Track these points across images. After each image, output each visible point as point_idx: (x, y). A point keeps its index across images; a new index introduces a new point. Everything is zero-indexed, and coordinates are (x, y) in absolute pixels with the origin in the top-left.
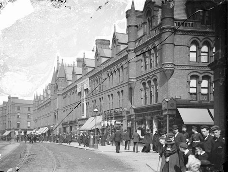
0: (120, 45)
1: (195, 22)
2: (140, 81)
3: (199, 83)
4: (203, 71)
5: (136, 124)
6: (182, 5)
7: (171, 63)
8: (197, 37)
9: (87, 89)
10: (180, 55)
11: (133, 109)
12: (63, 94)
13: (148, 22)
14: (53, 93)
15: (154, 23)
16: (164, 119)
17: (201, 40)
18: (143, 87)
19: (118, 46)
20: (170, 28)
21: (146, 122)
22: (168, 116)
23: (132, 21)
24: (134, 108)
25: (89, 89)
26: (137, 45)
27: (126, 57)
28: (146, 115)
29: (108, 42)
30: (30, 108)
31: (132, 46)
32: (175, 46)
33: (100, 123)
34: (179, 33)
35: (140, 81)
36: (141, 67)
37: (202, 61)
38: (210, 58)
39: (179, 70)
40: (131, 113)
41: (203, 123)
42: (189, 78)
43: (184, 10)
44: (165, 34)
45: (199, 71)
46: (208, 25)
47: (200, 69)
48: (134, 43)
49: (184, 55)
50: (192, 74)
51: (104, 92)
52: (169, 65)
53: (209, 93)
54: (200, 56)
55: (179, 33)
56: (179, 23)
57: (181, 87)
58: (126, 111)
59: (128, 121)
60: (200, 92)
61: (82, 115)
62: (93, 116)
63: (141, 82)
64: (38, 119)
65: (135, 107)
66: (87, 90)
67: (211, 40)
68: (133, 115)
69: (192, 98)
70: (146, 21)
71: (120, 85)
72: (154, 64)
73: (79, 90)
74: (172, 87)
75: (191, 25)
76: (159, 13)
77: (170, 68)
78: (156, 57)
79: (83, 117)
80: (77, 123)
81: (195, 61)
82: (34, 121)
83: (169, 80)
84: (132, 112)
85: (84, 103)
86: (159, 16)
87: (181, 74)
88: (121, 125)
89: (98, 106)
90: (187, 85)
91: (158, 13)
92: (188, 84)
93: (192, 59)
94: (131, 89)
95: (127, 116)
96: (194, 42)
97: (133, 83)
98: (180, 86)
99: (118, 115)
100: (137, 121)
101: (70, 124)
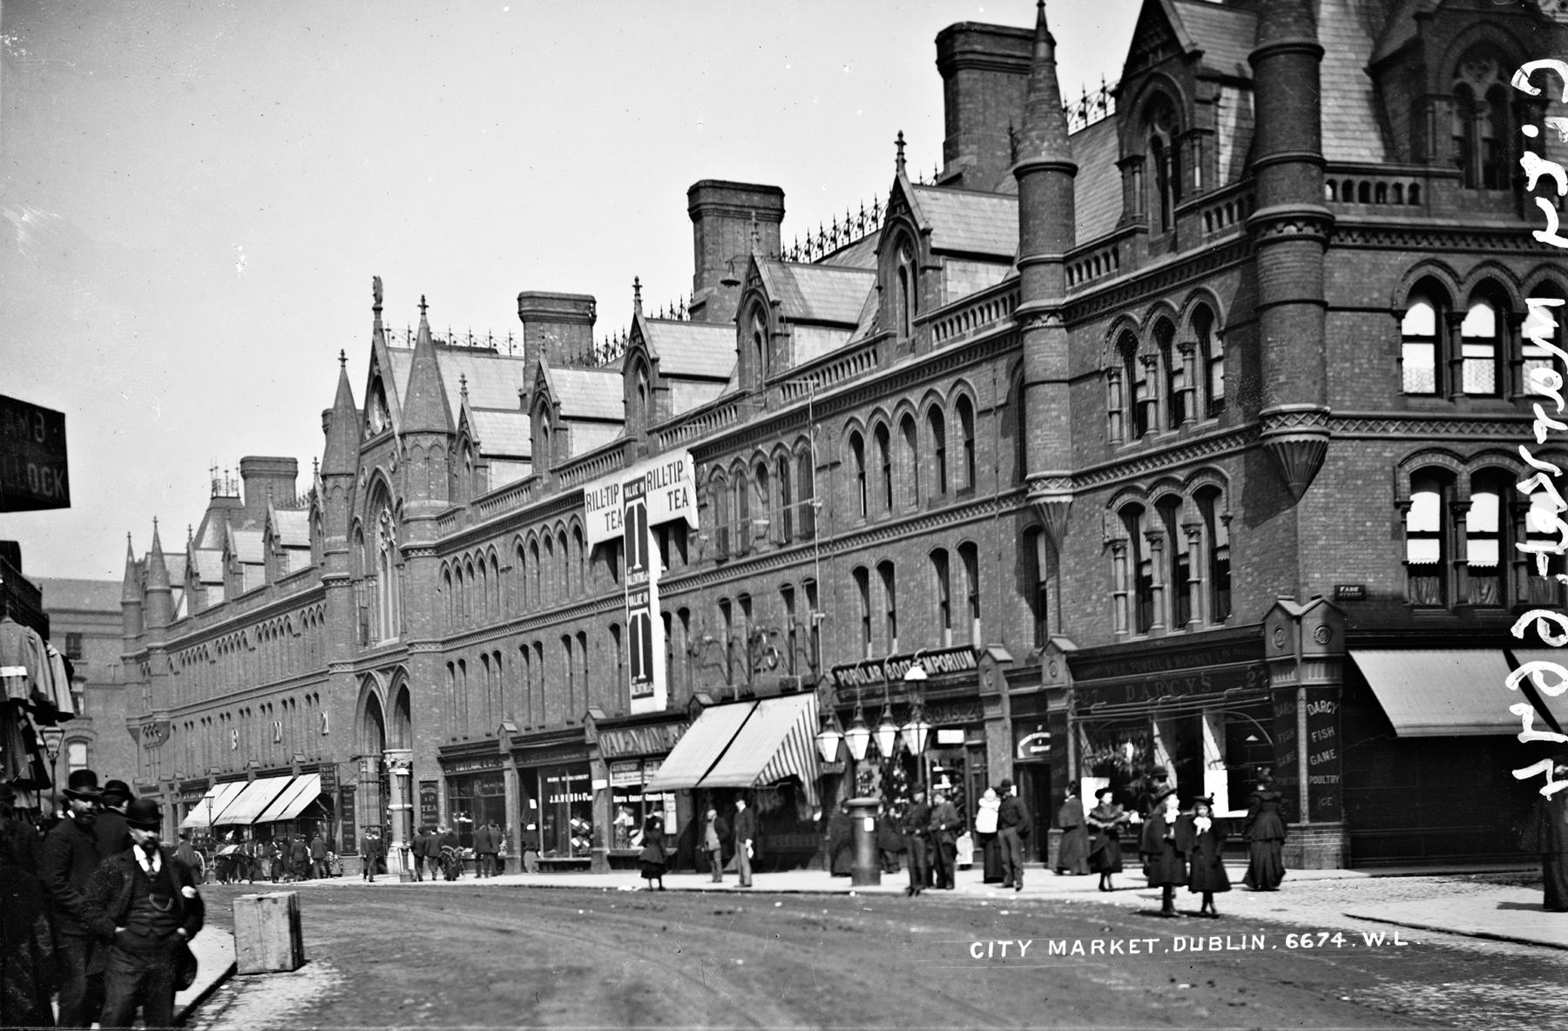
0: (940, 261)
1: (1427, 176)
2: (1106, 495)
3: (1454, 511)
4: (1477, 447)
5: (1084, 742)
6: (1351, 72)
7: (1313, 406)
8: (1442, 257)
9: (680, 525)
10: (1352, 361)
11: (1064, 657)
12: (440, 549)
13: (1150, 161)
14: (344, 538)
15: (1197, 170)
16: (1280, 712)
17: (1461, 272)
18: (1121, 531)
19: (930, 272)
20: (1310, 219)
21: (1156, 731)
22: (1302, 693)
23: (1042, 139)
24: (1065, 652)
25: (694, 522)
26: (1077, 283)
27: (1008, 345)
28: (1153, 689)
29: (773, 199)
30: (79, 636)
31: (1047, 291)
32: (1330, 314)
33: (814, 739)
34: (1349, 242)
35: (1106, 495)
36: (1111, 414)
37: (1467, 389)
38: (1507, 372)
39: (1348, 443)
40: (1047, 677)
41: (1492, 725)
42: (1405, 482)
43: (1365, 104)
44: (1279, 249)
45: (1454, 446)
46: (1494, 188)
47: (1461, 436)
48: (1060, 268)
49: (1375, 362)
50: (1417, 463)
51: (821, 545)
52: (1301, 417)
53: (1509, 563)
54: (1457, 363)
55: (1349, 242)
56: (1348, 186)
57: (1363, 533)
58: (1010, 667)
59: (1020, 725)
60: (1462, 560)
61: (633, 692)
62: (726, 700)
63: (1112, 500)
64: (179, 723)
65: (1075, 642)
66: (674, 532)
67: (1512, 276)
68: (1058, 693)
69: (1419, 594)
70: (1141, 153)
71: (952, 511)
72: (1194, 406)
73: (599, 526)
74: (1316, 538)
75: (1406, 194)
76: (1221, 111)
77: (1309, 438)
78: (1209, 364)
79: (639, 707)
80: (594, 746)
81: (1431, 388)
82: (134, 733)
83: (1303, 501)
84: (1057, 674)
85: (646, 619)
86: (1221, 129)
87: (1361, 466)
88: (964, 749)
89: (773, 634)
90: (1392, 523)
91: (1217, 115)
92: (1398, 517)
93: (1415, 383)
94: (1029, 537)
95: (1012, 697)
96: (1429, 290)
97: (1059, 503)
98: (1360, 528)
99: (948, 694)
100: (1086, 726)
101: (516, 753)
